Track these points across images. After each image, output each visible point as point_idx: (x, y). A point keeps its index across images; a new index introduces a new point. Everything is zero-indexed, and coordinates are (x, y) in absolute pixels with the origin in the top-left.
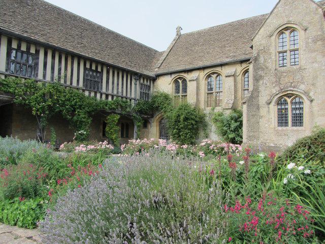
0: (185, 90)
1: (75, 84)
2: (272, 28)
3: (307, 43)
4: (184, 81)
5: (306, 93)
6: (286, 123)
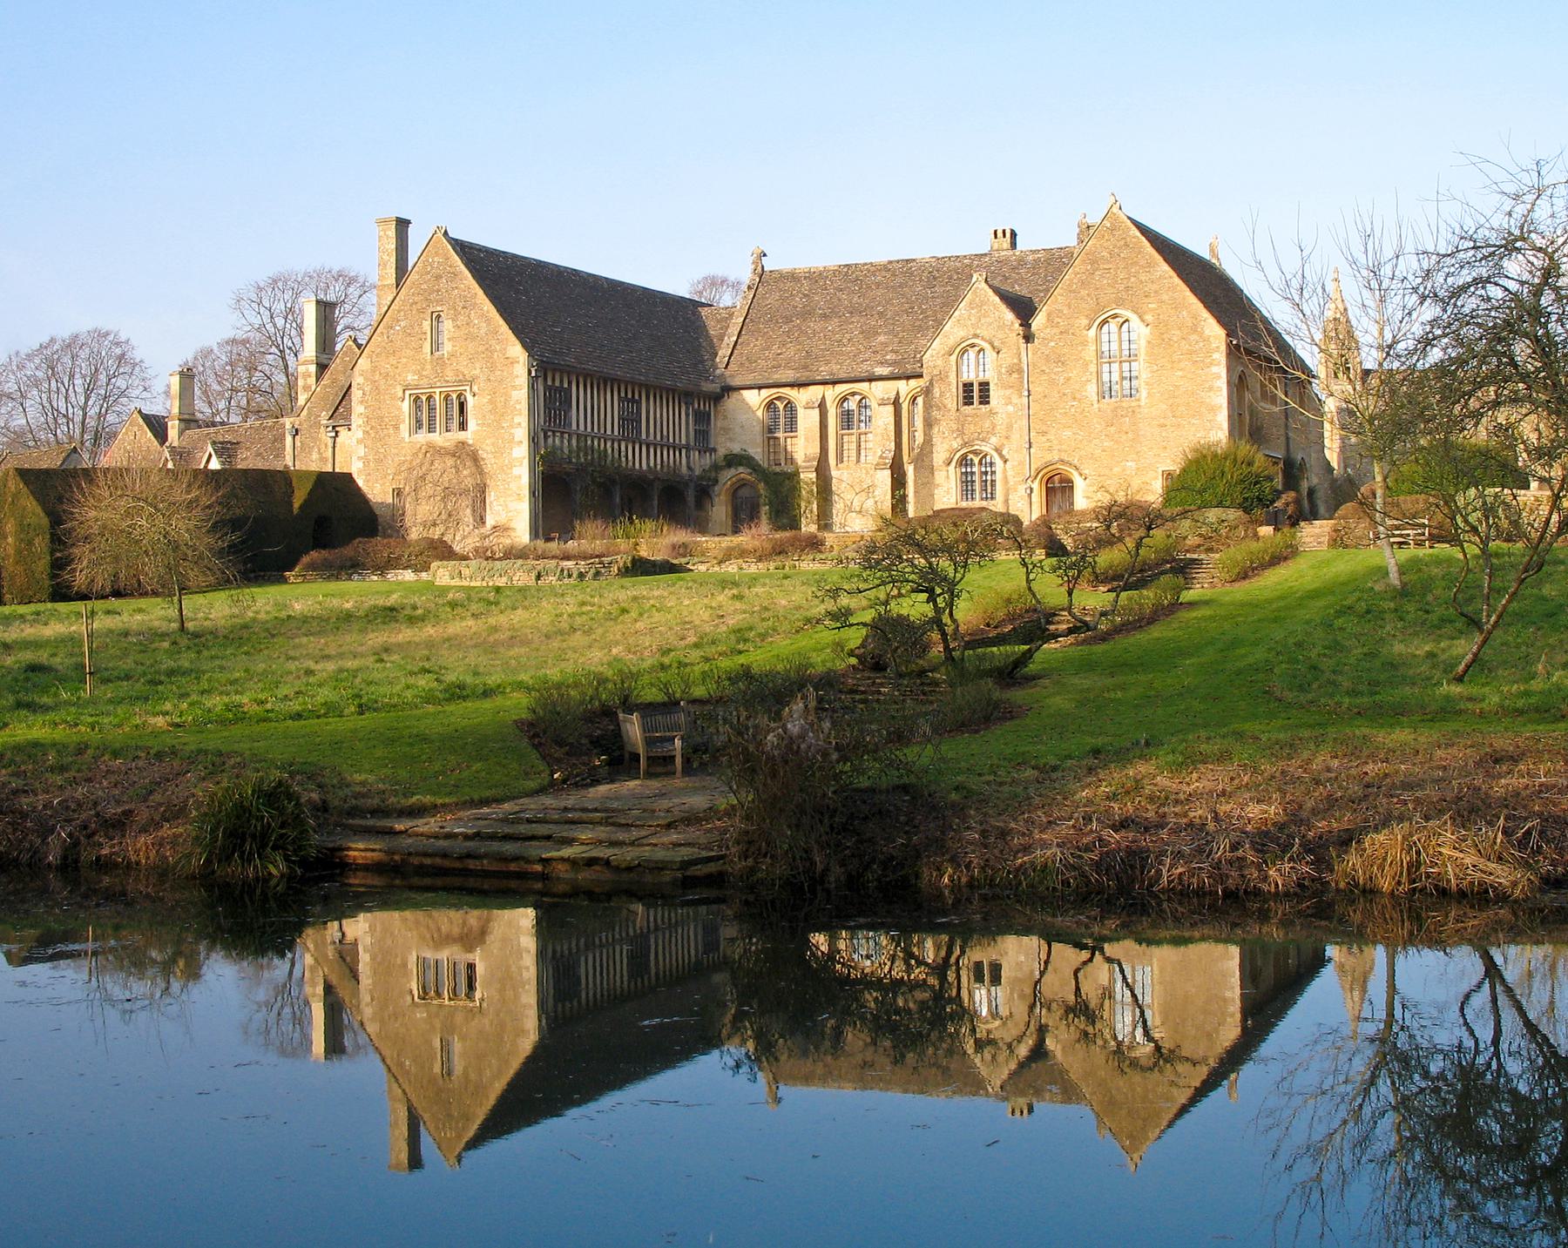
1: (582, 427)
2: (952, 342)
3: (1000, 373)
4: (790, 407)
6: (536, 735)
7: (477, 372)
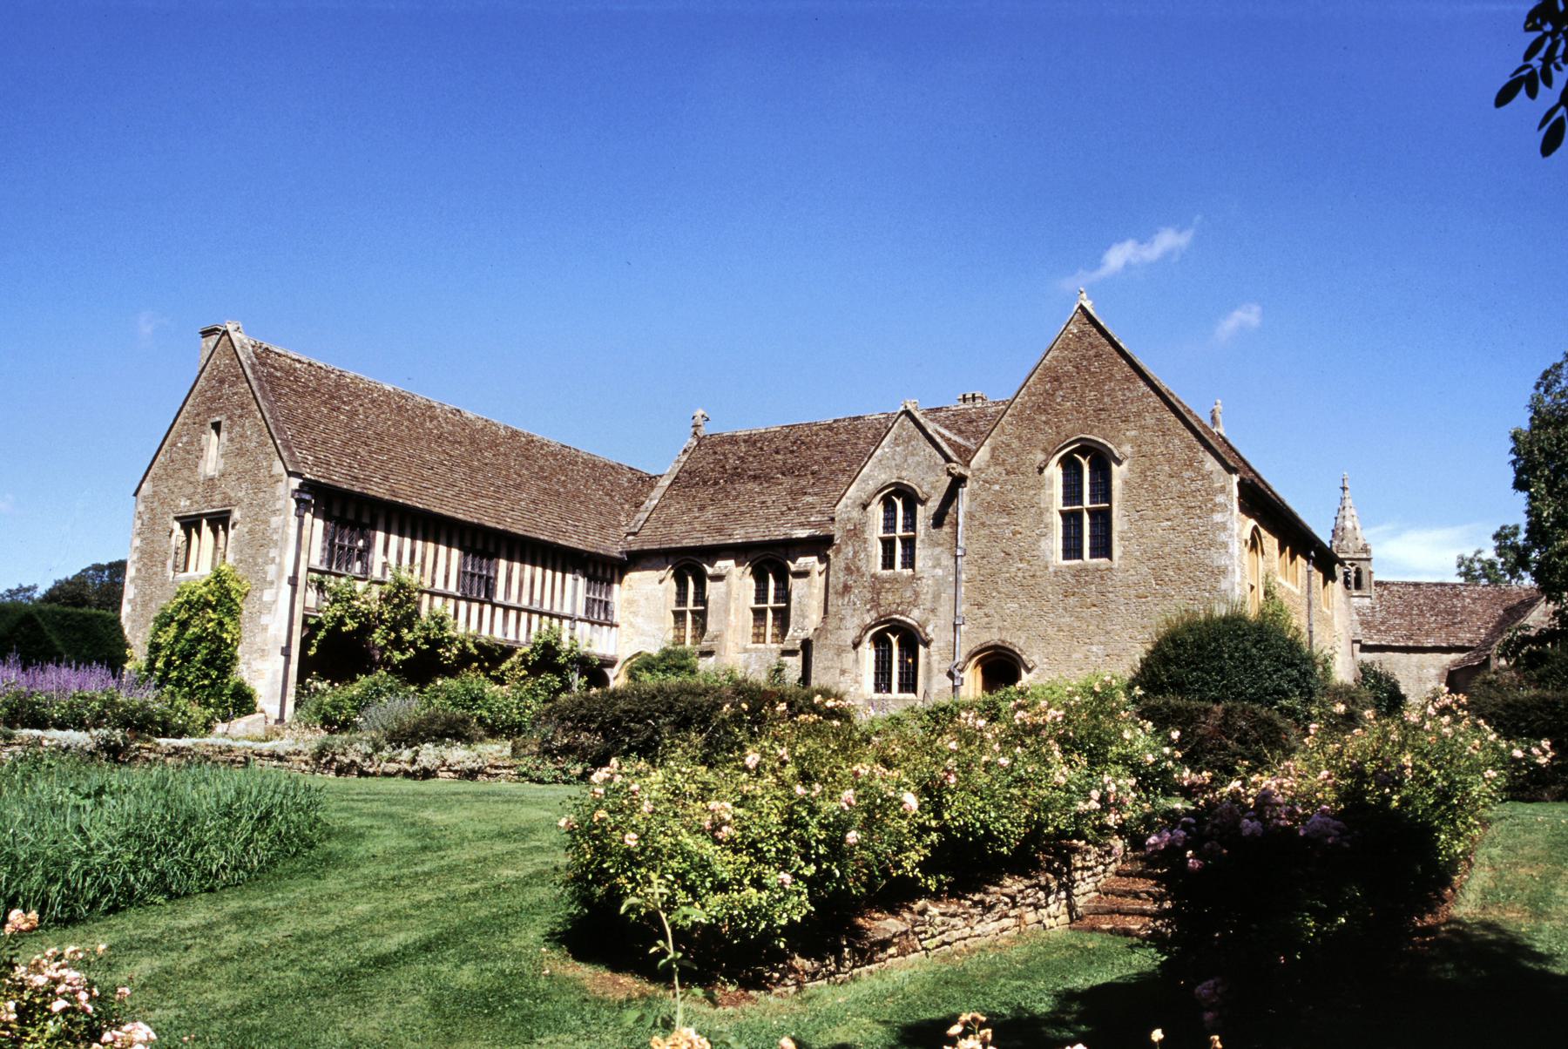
2: (872, 486)
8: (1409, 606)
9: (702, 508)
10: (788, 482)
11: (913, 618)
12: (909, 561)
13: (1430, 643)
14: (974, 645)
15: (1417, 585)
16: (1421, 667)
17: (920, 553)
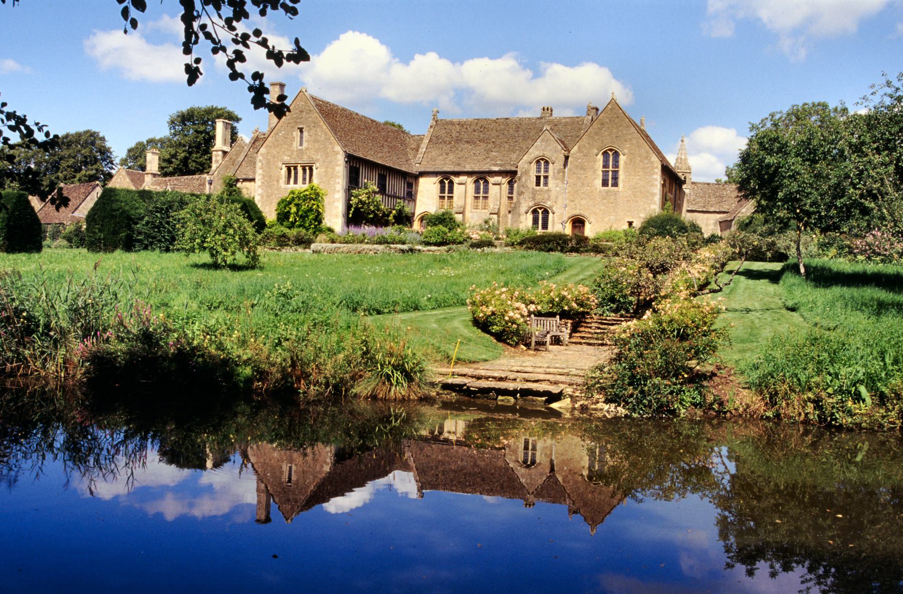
0: (451, 191)
2: (532, 156)
4: (451, 183)
5: (551, 208)
7: (319, 157)
8: (705, 193)
9: (447, 154)
10: (483, 145)
11: (548, 204)
12: (546, 184)
13: (712, 209)
14: (570, 215)
15: (708, 184)
16: (707, 219)
17: (550, 180)
